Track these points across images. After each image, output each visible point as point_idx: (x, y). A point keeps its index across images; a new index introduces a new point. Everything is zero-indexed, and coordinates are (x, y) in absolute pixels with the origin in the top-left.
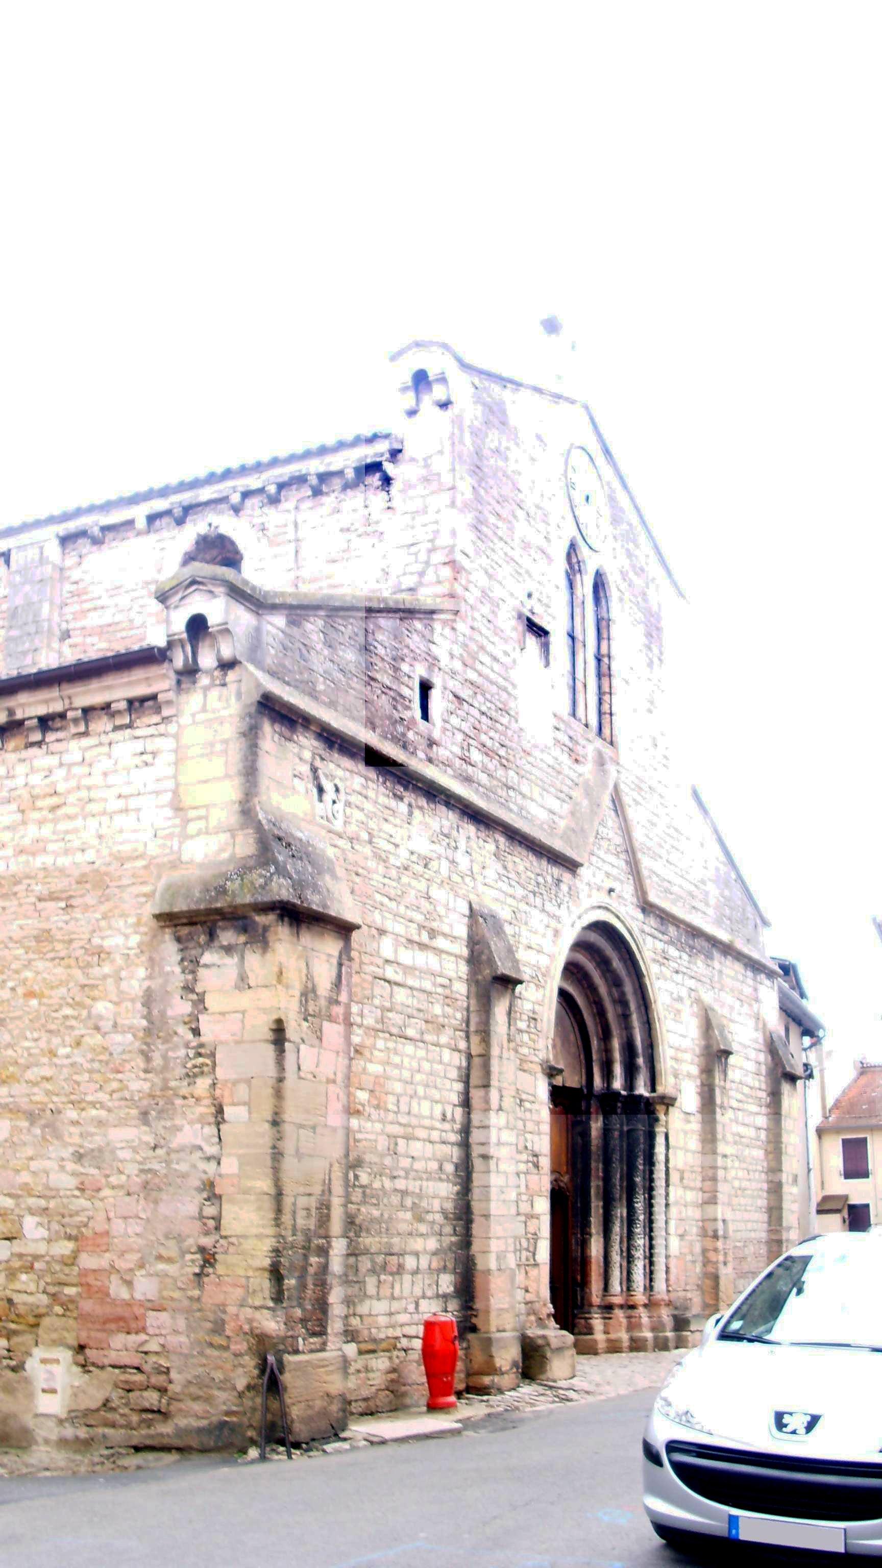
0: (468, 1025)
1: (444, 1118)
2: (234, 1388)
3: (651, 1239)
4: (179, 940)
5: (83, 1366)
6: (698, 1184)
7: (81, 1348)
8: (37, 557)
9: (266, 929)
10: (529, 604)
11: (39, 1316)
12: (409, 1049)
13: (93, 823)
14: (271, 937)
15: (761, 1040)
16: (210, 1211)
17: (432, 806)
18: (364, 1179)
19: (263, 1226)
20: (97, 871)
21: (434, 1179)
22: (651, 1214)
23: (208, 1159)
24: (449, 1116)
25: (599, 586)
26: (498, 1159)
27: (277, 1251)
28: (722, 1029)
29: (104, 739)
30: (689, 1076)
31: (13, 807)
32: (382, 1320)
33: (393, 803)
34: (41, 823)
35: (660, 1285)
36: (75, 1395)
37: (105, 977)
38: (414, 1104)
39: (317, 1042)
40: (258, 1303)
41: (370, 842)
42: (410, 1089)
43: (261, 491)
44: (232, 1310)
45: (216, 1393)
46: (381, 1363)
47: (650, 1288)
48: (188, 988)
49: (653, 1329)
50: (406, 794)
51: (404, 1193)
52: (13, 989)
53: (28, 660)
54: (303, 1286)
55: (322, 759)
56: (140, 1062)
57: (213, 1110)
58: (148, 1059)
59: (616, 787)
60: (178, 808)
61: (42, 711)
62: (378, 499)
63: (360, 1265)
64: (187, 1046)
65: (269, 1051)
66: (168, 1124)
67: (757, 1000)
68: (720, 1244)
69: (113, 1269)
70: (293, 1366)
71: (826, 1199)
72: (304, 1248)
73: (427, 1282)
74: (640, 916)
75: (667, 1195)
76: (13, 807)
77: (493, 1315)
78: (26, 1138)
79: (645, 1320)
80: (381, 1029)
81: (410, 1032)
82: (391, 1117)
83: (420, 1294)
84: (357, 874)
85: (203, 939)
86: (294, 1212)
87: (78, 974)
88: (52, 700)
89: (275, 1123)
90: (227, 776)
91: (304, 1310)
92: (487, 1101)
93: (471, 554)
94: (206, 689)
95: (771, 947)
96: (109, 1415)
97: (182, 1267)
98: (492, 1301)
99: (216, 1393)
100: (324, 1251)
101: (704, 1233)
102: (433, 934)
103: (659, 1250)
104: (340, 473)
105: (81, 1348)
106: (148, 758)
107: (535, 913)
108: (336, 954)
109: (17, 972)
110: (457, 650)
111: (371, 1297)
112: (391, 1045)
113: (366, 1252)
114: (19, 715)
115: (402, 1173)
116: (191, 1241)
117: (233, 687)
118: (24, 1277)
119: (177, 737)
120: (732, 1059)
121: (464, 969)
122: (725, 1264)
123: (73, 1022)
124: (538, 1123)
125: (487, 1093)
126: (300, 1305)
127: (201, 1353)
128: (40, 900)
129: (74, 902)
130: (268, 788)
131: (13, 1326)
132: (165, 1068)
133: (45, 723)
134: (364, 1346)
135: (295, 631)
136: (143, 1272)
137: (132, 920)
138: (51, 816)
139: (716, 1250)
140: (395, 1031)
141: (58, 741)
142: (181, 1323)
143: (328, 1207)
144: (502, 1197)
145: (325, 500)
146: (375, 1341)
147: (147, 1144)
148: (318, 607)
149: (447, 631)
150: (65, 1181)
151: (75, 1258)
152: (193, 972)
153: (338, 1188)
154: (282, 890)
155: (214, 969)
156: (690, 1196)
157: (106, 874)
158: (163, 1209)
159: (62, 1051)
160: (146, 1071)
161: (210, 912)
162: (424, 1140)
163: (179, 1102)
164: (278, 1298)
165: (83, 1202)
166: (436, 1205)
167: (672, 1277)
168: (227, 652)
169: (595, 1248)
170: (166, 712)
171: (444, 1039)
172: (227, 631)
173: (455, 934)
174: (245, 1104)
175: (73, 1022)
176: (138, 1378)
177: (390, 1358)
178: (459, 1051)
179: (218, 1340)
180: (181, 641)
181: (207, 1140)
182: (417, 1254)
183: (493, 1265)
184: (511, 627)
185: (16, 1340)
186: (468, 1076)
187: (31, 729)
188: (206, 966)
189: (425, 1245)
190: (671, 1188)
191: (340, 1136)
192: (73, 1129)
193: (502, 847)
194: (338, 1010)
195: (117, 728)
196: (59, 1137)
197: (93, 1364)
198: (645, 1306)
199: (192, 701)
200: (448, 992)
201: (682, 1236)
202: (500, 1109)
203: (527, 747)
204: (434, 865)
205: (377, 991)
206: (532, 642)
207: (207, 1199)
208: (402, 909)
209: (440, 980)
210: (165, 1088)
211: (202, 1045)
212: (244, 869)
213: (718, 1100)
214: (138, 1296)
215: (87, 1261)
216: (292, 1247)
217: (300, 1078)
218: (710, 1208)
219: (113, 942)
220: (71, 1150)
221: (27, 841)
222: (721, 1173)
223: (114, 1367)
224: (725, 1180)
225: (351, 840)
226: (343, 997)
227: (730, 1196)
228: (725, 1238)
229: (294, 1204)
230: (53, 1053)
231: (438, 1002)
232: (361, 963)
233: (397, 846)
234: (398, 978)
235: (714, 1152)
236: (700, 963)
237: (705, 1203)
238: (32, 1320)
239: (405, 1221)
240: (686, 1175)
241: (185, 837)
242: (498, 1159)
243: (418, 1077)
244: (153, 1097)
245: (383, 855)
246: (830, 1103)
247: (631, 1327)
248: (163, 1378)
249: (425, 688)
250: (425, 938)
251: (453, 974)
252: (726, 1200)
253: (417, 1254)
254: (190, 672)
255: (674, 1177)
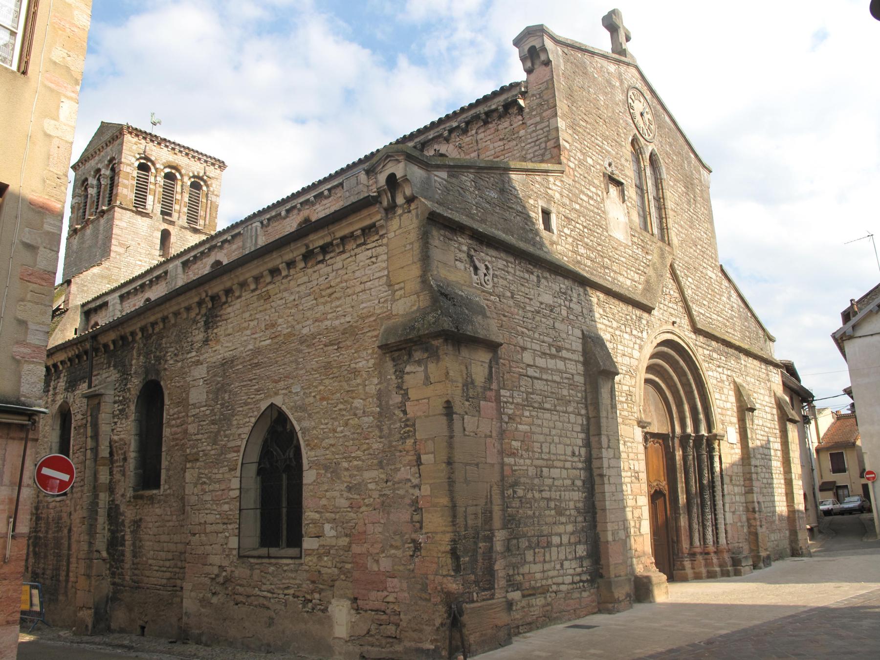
0: (586, 400)
1: (573, 454)
2: (434, 625)
3: (715, 515)
4: (393, 360)
5: (357, 610)
6: (742, 483)
7: (356, 599)
8: (355, 182)
9: (437, 348)
10: (609, 169)
11: (333, 581)
12: (547, 415)
13: (348, 300)
14: (441, 352)
15: (773, 402)
16: (417, 518)
17: (553, 276)
18: (520, 493)
19: (446, 526)
20: (351, 326)
21: (569, 490)
22: (714, 501)
23: (414, 487)
24: (577, 453)
25: (653, 160)
26: (609, 476)
27: (454, 541)
28: (749, 396)
29: (353, 253)
30: (731, 423)
31: (312, 297)
32: (538, 576)
33: (527, 276)
34: (324, 304)
35: (722, 540)
36: (353, 627)
37: (358, 385)
38: (552, 446)
39: (477, 414)
40: (444, 573)
41: (512, 297)
42: (549, 439)
43: (458, 127)
44: (431, 577)
45: (425, 627)
46: (539, 601)
47: (716, 542)
48: (399, 387)
49: (720, 566)
50: (535, 270)
51: (549, 500)
52: (314, 397)
53: (717, 396)
54: (474, 560)
55: (475, 251)
56: (377, 433)
57: (415, 458)
58: (381, 430)
59: (671, 266)
60: (390, 285)
61: (321, 243)
62: (517, 121)
63: (520, 545)
64: (400, 420)
65: (444, 420)
66: (393, 467)
67: (769, 380)
68: (757, 515)
69: (369, 554)
70: (469, 611)
71: (824, 483)
72: (474, 538)
73: (568, 550)
74: (694, 337)
75: (723, 490)
76: (312, 297)
77: (612, 568)
78: (325, 479)
79: (715, 561)
80: (528, 404)
81: (547, 406)
82: (537, 455)
83: (564, 557)
84: (505, 316)
85: (406, 357)
86: (466, 516)
87: (344, 384)
88: (325, 236)
89: (450, 463)
90: (414, 263)
91: (476, 575)
92: (600, 443)
93: (570, 141)
94: (400, 216)
95: (779, 356)
96: (370, 639)
97: (404, 552)
98: (611, 559)
99: (425, 627)
100: (490, 539)
101: (747, 510)
102: (559, 349)
103: (721, 521)
104: (496, 110)
105: (355, 600)
106: (374, 260)
107: (626, 336)
108: (488, 361)
109: (316, 387)
110: (566, 192)
111: (530, 563)
112: (534, 413)
113: (525, 536)
114: (311, 247)
115: (547, 488)
116: (407, 536)
117: (414, 212)
118: (326, 558)
119: (387, 245)
120: (756, 413)
121: (581, 368)
122: (761, 526)
123: (344, 413)
124: (637, 454)
125: (600, 439)
126: (473, 573)
127: (416, 603)
128: (326, 346)
129: (341, 345)
130: (437, 267)
131: (321, 586)
132: (390, 434)
133: (325, 249)
134: (526, 592)
135: (454, 180)
136: (384, 555)
137: (370, 351)
138: (329, 299)
139: (755, 519)
140: (536, 405)
141: (331, 258)
142: (405, 585)
143: (491, 512)
144: (613, 498)
145: (490, 126)
146: (534, 588)
147: (383, 479)
148: (468, 167)
149: (558, 183)
150: (343, 503)
151: (350, 547)
152: (402, 378)
153: (497, 500)
154: (447, 324)
155: (412, 375)
156: (736, 489)
157: (356, 327)
158: (392, 517)
159: (339, 429)
160: (380, 437)
161: (406, 341)
162: (561, 468)
163: (398, 454)
164: (457, 569)
165: (352, 515)
166: (572, 505)
167: (729, 535)
168: (408, 192)
169: (683, 521)
170: (381, 233)
171: (570, 409)
172: (407, 179)
173: (574, 348)
174: (432, 453)
175: (344, 413)
176: (384, 617)
177: (545, 598)
178: (581, 415)
179: (424, 595)
180: (384, 190)
181: (413, 475)
182: (560, 535)
183: (610, 538)
184: (599, 181)
185: (323, 594)
186: (588, 429)
187: (317, 254)
188: (408, 373)
189: (565, 530)
190: (725, 486)
191: (497, 468)
192: (346, 473)
193: (602, 299)
194: (491, 394)
195: (359, 246)
196: (339, 478)
197: (362, 609)
198: (715, 552)
199: (394, 224)
200: (571, 381)
201: (734, 513)
202: (609, 447)
203: (615, 245)
204: (557, 310)
205: (522, 383)
206: (613, 190)
207: (415, 511)
208: (536, 335)
209: (565, 375)
210: (391, 446)
211: (408, 420)
212: (424, 313)
213: (749, 436)
214: (382, 569)
215: (356, 549)
216: (465, 538)
217: (465, 435)
218: (750, 496)
219: (362, 364)
220: (345, 485)
221: (318, 315)
222: (754, 476)
223: (372, 610)
224: (758, 480)
225: (499, 296)
226: (494, 386)
227: (761, 488)
228: (760, 512)
229: (465, 512)
230: (335, 431)
231: (565, 387)
232: (510, 367)
233: (531, 299)
234: (537, 375)
235: (750, 465)
236: (733, 362)
237: (746, 493)
238: (331, 583)
239: (550, 516)
240: (734, 478)
241: (394, 301)
242: (609, 476)
243: (554, 432)
244: (384, 452)
245: (522, 305)
246: (821, 435)
247: (706, 565)
248: (397, 617)
249: (546, 214)
250: (553, 351)
251: (575, 372)
252: (759, 490)
253: (560, 535)
254: (391, 209)
255: (726, 480)
